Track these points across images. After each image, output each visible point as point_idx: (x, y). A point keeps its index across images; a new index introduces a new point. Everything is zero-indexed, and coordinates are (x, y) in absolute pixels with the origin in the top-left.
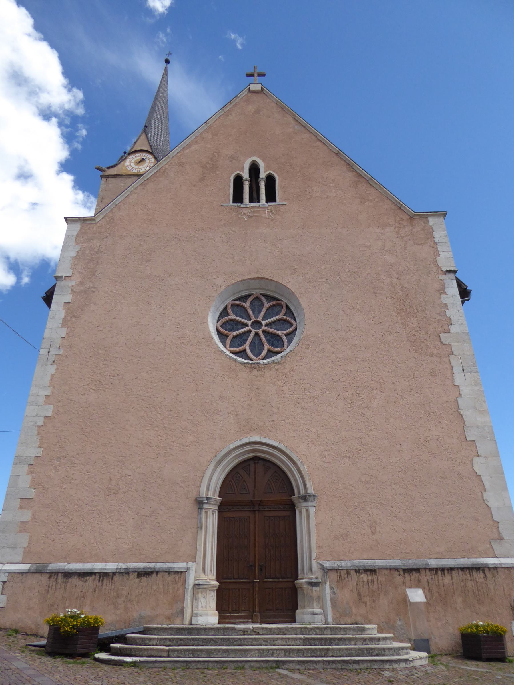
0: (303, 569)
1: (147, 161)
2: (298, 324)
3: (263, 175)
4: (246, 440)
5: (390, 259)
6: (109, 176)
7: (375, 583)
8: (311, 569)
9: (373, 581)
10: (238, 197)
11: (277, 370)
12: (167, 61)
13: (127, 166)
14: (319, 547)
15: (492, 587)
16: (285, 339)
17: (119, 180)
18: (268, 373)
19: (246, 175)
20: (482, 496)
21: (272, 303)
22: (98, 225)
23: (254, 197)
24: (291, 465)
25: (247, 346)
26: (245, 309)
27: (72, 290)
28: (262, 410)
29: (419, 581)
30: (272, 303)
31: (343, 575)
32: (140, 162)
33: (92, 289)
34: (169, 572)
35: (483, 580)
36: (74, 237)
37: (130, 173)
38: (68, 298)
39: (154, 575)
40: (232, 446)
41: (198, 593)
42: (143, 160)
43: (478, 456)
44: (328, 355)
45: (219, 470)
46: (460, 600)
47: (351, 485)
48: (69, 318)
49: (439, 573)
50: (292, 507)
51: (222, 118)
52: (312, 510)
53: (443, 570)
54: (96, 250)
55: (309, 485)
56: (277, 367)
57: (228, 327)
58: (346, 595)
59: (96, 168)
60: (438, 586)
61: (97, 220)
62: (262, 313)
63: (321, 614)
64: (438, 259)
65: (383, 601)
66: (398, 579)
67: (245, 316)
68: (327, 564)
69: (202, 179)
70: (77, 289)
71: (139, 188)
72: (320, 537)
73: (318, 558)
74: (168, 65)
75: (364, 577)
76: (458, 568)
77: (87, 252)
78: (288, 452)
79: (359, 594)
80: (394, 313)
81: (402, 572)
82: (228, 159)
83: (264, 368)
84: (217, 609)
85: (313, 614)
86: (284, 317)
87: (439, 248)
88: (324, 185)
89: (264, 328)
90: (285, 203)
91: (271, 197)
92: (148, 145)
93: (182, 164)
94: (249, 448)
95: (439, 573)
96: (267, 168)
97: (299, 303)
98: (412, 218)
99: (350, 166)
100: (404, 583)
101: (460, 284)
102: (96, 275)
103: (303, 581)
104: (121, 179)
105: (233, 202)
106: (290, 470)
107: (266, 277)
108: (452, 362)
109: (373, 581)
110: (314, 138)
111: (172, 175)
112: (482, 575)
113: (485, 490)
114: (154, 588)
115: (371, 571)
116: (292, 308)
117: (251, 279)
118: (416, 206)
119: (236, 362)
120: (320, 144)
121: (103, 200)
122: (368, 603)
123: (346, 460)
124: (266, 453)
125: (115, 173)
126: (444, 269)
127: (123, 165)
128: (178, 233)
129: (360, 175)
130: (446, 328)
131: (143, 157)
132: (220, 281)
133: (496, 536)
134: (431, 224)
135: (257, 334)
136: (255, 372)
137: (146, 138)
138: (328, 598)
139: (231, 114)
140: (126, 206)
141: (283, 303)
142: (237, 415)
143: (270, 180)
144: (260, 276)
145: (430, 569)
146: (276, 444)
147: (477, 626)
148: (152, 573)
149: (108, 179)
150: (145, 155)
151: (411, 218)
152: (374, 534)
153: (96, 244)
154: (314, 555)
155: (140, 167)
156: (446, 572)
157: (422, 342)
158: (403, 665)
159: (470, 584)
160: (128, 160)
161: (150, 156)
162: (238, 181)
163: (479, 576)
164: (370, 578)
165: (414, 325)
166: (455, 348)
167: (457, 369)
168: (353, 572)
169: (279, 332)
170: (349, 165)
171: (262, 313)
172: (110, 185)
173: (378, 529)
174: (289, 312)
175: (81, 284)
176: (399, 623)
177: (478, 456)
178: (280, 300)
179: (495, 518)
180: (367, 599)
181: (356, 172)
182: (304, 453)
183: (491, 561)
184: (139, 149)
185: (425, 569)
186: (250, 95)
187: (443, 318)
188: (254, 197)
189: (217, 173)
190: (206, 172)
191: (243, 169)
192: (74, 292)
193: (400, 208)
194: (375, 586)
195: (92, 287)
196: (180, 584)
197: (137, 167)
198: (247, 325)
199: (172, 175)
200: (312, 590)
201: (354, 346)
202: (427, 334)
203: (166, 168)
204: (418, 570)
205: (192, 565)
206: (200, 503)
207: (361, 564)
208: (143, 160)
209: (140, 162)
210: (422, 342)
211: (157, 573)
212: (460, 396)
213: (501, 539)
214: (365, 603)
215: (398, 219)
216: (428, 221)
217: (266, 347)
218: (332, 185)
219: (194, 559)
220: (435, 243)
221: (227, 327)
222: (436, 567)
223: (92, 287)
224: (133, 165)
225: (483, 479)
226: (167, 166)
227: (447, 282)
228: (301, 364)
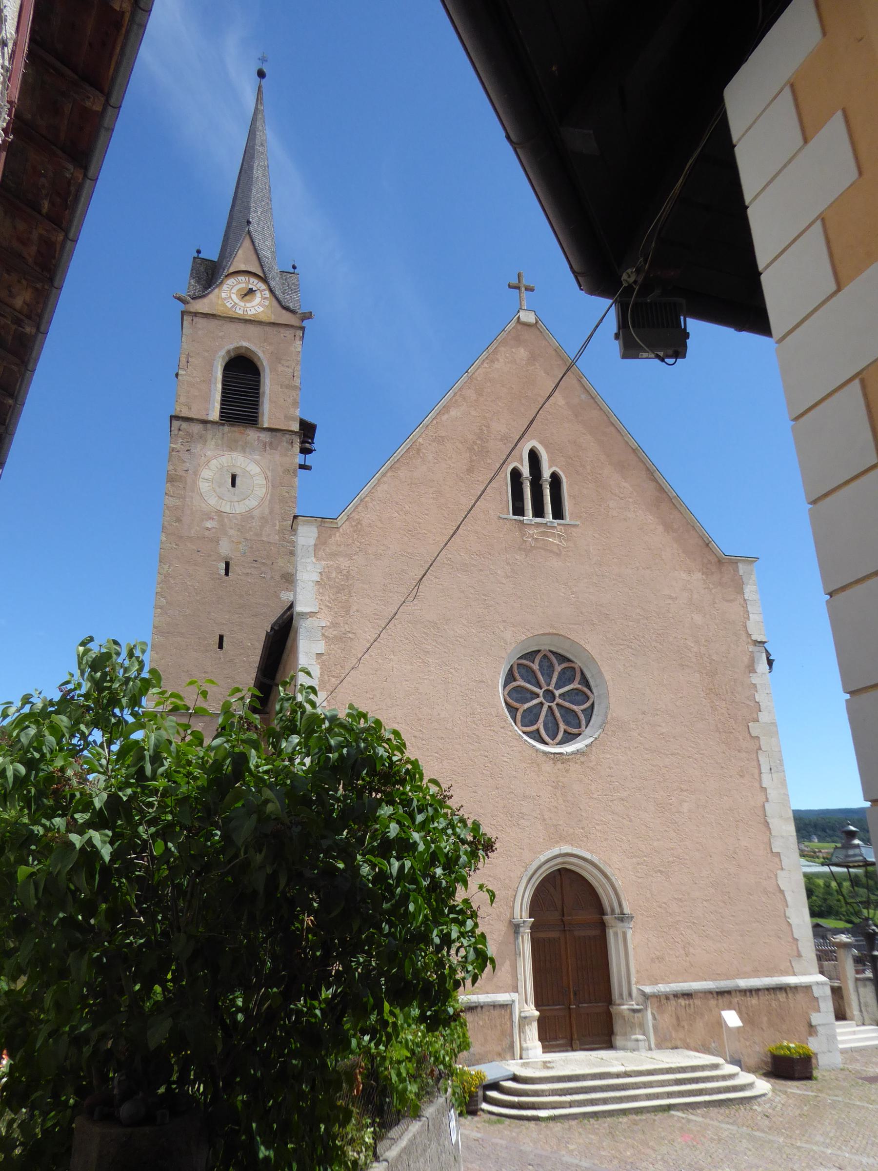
0: (621, 995)
1: (258, 294)
2: (596, 695)
3: (546, 474)
4: (556, 851)
5: (698, 619)
6: (196, 314)
7: (692, 1006)
8: (630, 995)
9: (689, 1005)
10: (518, 510)
11: (582, 763)
12: (261, 74)
13: (225, 299)
14: (638, 972)
15: (792, 1006)
16: (582, 717)
17: (214, 323)
18: (574, 767)
19: (526, 471)
20: (785, 914)
21: (563, 666)
22: (341, 530)
23: (539, 512)
24: (604, 881)
25: (540, 725)
26: (533, 672)
27: (323, 635)
28: (570, 813)
29: (731, 1002)
30: (563, 666)
31: (662, 999)
32: (246, 295)
33: (350, 635)
34: (495, 1006)
35: (785, 1000)
36: (311, 549)
37: (231, 314)
38: (320, 647)
39: (479, 1009)
40: (543, 859)
41: (524, 1026)
42: (251, 291)
43: (782, 869)
44: (636, 745)
45: (530, 886)
46: (765, 1019)
47: (665, 903)
48: (326, 677)
49: (748, 993)
50: (603, 927)
51: (486, 365)
52: (630, 933)
53: (750, 991)
54: (345, 572)
55: (625, 904)
56: (582, 759)
57: (515, 695)
58: (667, 1019)
59: (175, 298)
60: (747, 1007)
61: (340, 524)
62: (554, 680)
63: (644, 1040)
64: (748, 623)
65: (700, 1025)
66: (713, 1002)
67: (533, 681)
68: (648, 989)
69: (470, 470)
70: (331, 633)
71: (389, 474)
72: (640, 960)
73: (637, 983)
74: (264, 81)
75: (682, 1002)
76: (764, 989)
77: (334, 575)
78: (601, 866)
79: (678, 1018)
80: (703, 694)
81: (715, 995)
82: (501, 440)
83: (568, 760)
84: (540, 1039)
85: (637, 1040)
86: (579, 686)
87: (750, 608)
88: (621, 499)
89: (558, 700)
90: (577, 523)
91: (558, 513)
92: (257, 263)
93: (440, 440)
94: (560, 860)
95: (748, 993)
96: (552, 463)
97: (600, 672)
98: (720, 562)
99: (651, 474)
100: (717, 1005)
101: (768, 654)
102: (351, 613)
103: (625, 1007)
104: (216, 322)
105: (514, 514)
106: (605, 890)
107: (561, 633)
108: (760, 759)
109: (689, 1005)
110: (605, 418)
111: (430, 457)
112: (784, 995)
113: (787, 906)
114: (481, 1023)
115: (688, 995)
116: (588, 675)
117: (542, 634)
118: (727, 546)
119: (537, 750)
120: (612, 429)
121: (190, 360)
122: (686, 1027)
123: (659, 874)
124: (575, 865)
125: (206, 310)
126: (754, 638)
127: (219, 297)
128: (450, 556)
129: (661, 489)
130: (755, 716)
131: (250, 286)
132: (508, 635)
133: (795, 954)
134: (741, 572)
135: (542, 704)
136: (559, 765)
137: (251, 247)
138: (650, 1025)
139: (498, 360)
140: (374, 503)
141: (576, 666)
142: (544, 820)
143: (556, 480)
144: (554, 631)
145: (740, 991)
146: (588, 856)
147: (789, 1049)
148: (476, 1007)
149: (196, 319)
150: (254, 283)
151: (719, 561)
152: (687, 956)
153: (344, 563)
154: (633, 980)
155: (248, 305)
156: (754, 993)
157: (731, 733)
158: (763, 1098)
159: (774, 1004)
160: (225, 287)
161: (262, 286)
162: (516, 475)
163: (782, 996)
164: (687, 1002)
165: (723, 711)
166: (763, 742)
167: (765, 768)
168: (671, 997)
169: (575, 708)
170: (648, 469)
171: (554, 680)
172: (200, 332)
173: (691, 950)
174: (585, 681)
175: (334, 625)
176: (713, 1045)
177: (782, 869)
178: (572, 662)
179: (795, 936)
180: (685, 1024)
181: (657, 482)
182: (617, 866)
183: (792, 980)
184: (243, 267)
185: (736, 991)
186: (519, 327)
187: (752, 704)
188: (539, 512)
189: (489, 461)
190: (475, 458)
191: (521, 461)
192: (326, 637)
193: (707, 545)
194: (692, 1010)
195: (349, 632)
196: (507, 1017)
197: (242, 304)
198: (538, 696)
199: (430, 457)
200: (634, 1017)
201: (662, 734)
202: (736, 723)
203: (420, 444)
204: (729, 992)
205: (515, 996)
206: (516, 928)
207: (679, 989)
208: (251, 291)
209: (246, 295)
210: (731, 733)
211: (482, 1007)
212: (767, 800)
213: (799, 955)
214: (683, 1027)
215: (705, 561)
216: (737, 567)
217: (562, 727)
218: (631, 500)
219: (515, 989)
220: (745, 600)
221: (516, 696)
222: (745, 988)
223: (349, 632)
224: (234, 297)
225: (787, 894)
226: (420, 440)
227: (756, 655)
228: (608, 756)
